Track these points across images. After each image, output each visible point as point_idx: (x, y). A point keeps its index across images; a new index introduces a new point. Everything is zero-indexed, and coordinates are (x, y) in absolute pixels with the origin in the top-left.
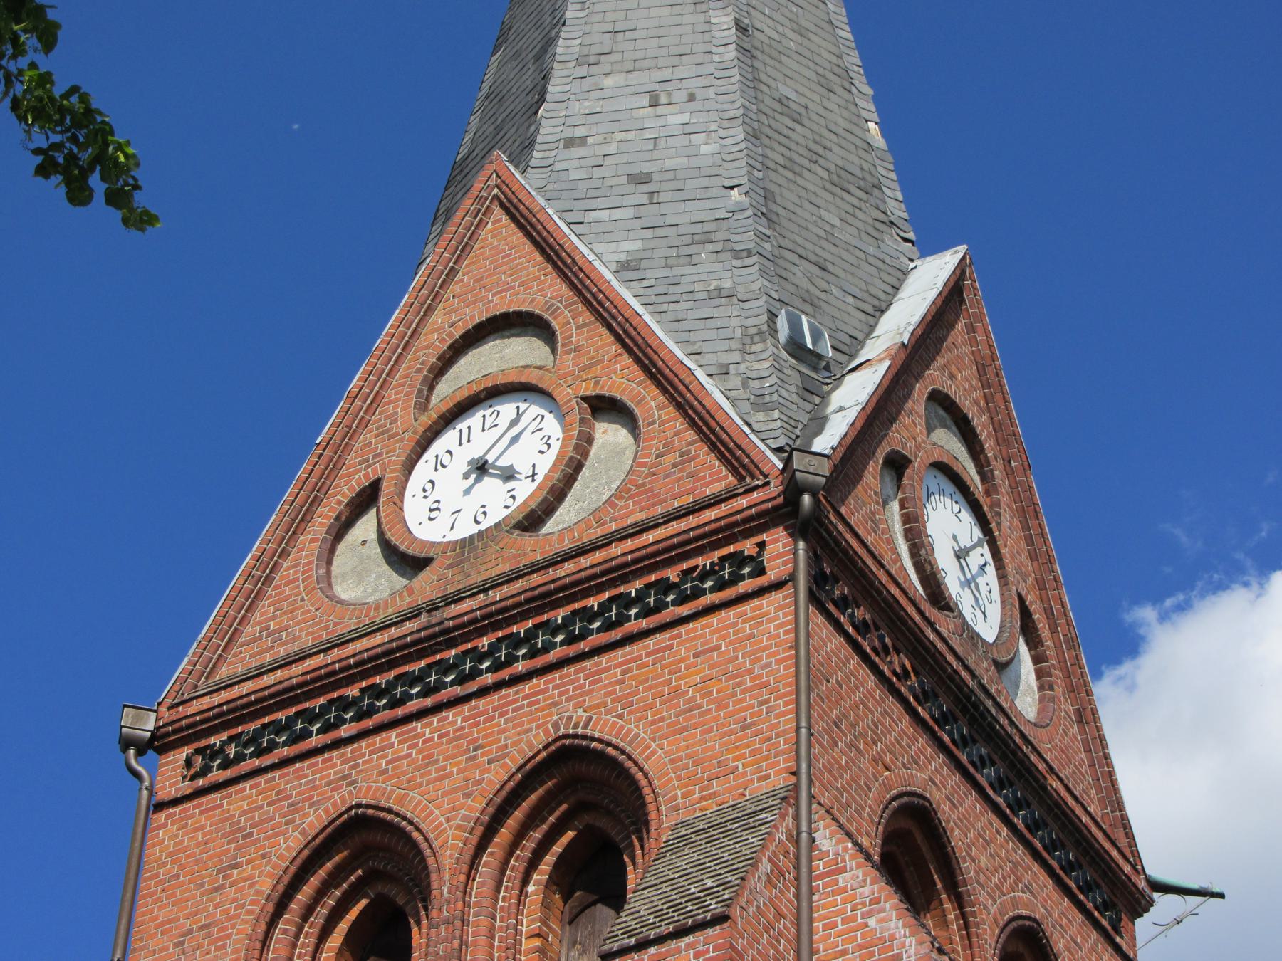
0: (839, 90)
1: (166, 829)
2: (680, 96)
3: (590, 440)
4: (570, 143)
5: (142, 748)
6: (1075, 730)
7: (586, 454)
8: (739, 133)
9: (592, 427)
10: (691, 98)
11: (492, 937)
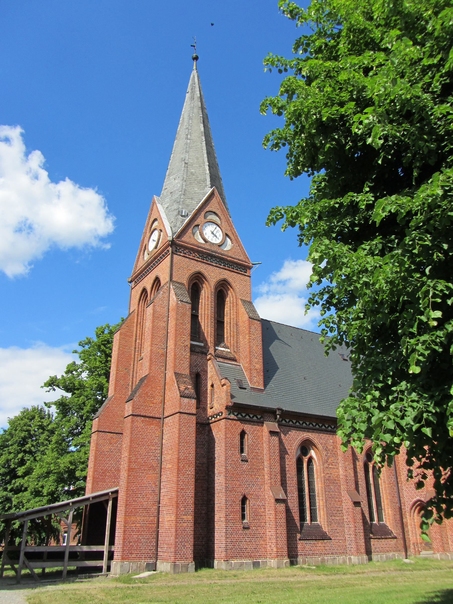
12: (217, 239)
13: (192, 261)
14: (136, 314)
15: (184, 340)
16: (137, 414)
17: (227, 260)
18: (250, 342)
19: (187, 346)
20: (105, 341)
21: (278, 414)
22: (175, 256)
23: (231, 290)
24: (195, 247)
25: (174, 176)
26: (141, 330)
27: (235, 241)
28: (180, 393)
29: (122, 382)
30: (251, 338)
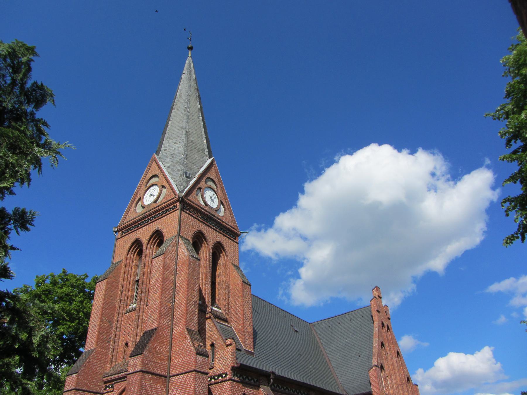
0: (201, 137)
1: (119, 242)
2: (178, 142)
3: (162, 191)
4: (165, 150)
5: (116, 232)
6: (230, 215)
7: (161, 193)
8: (184, 147)
9: (162, 189)
10: (179, 142)
11: (150, 253)
12: (214, 204)
13: (196, 220)
14: (123, 264)
15: (194, 296)
16: (146, 370)
17: (222, 225)
18: (243, 305)
19: (196, 301)
20: (46, 290)
21: (272, 378)
23: (224, 253)
24: (199, 208)
25: (174, 141)
26: (129, 281)
28: (196, 349)
29: (104, 335)
30: (244, 301)
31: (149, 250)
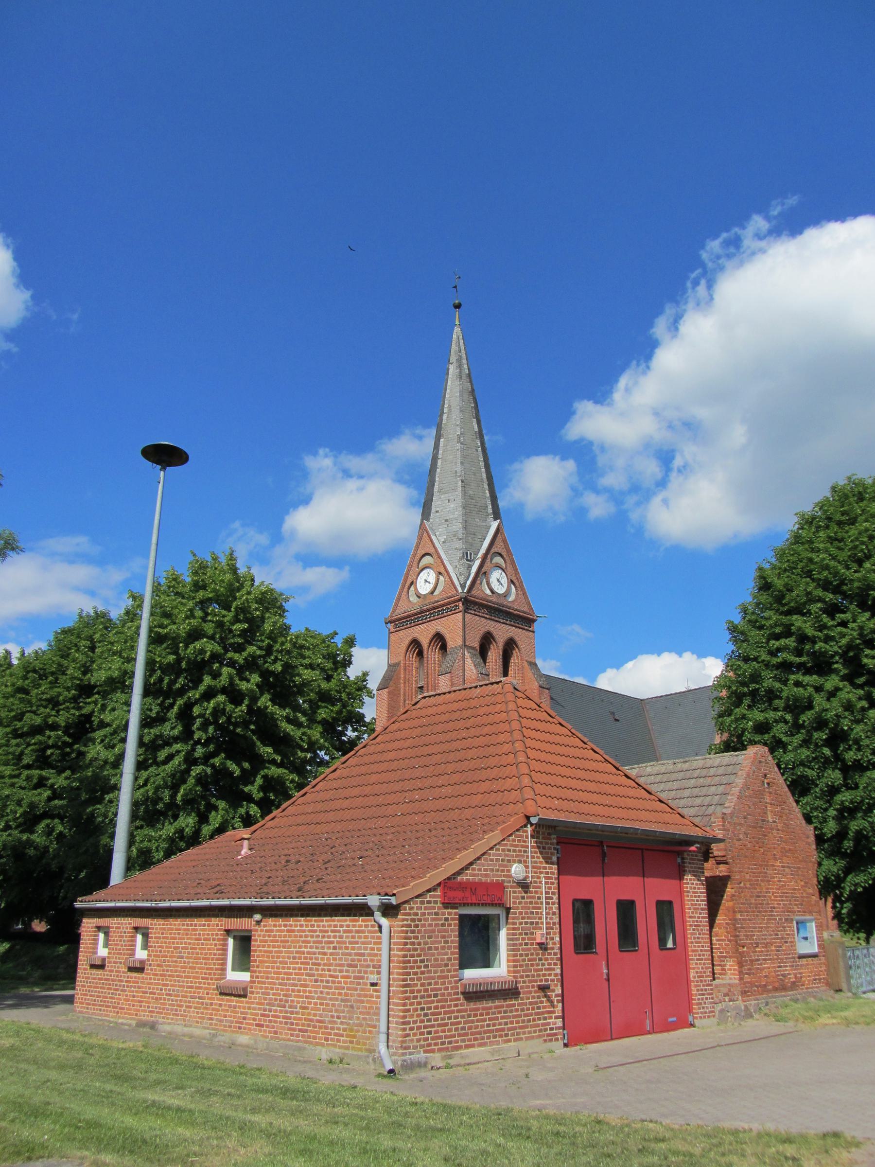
4: (437, 512)
13: (482, 619)
22: (467, 615)
27: (520, 587)
31: (432, 655)
